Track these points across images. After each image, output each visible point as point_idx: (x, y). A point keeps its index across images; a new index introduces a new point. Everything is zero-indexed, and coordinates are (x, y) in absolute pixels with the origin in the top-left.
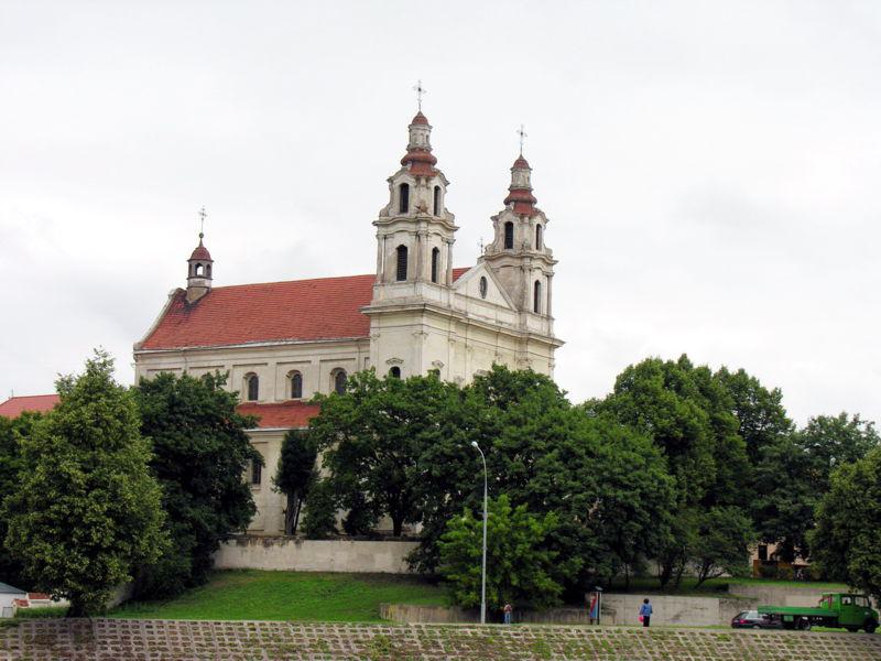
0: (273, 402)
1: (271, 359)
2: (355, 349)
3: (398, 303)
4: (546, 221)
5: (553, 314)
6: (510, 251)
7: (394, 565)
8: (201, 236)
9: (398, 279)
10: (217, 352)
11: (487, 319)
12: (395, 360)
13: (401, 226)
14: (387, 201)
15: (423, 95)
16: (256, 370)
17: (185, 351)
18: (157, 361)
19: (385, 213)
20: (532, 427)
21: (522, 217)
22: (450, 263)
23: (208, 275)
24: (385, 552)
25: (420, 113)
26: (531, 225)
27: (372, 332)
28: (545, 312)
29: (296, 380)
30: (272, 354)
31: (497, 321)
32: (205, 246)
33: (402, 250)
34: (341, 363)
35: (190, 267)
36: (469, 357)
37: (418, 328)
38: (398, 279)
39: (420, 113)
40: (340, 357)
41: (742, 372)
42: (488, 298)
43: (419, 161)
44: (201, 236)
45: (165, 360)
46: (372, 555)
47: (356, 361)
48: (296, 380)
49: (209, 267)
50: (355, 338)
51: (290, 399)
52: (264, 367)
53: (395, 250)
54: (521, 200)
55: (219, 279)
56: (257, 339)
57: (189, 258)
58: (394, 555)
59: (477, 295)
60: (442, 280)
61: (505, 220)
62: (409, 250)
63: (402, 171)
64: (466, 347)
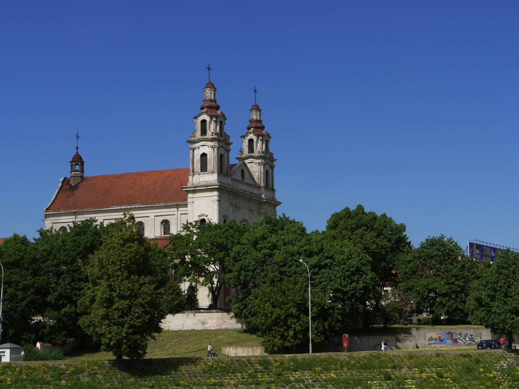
0: (154, 237)
1: (151, 213)
3: (202, 184)
4: (225, 119)
5: (275, 188)
6: (252, 154)
8: (77, 148)
9: (201, 172)
11: (245, 191)
12: (202, 215)
15: (210, 72)
17: (74, 212)
18: (58, 218)
20: (56, 294)
22: (228, 162)
27: (189, 200)
28: (271, 187)
29: (166, 224)
31: (250, 192)
34: (167, 217)
35: (72, 165)
36: (238, 212)
38: (201, 172)
40: (166, 214)
41: (384, 215)
42: (245, 181)
44: (77, 148)
47: (176, 215)
48: (166, 224)
49: (82, 165)
50: (175, 203)
51: (163, 235)
53: (200, 156)
56: (116, 205)
57: (71, 161)
59: (240, 178)
60: (225, 171)
62: (208, 156)
64: (236, 207)
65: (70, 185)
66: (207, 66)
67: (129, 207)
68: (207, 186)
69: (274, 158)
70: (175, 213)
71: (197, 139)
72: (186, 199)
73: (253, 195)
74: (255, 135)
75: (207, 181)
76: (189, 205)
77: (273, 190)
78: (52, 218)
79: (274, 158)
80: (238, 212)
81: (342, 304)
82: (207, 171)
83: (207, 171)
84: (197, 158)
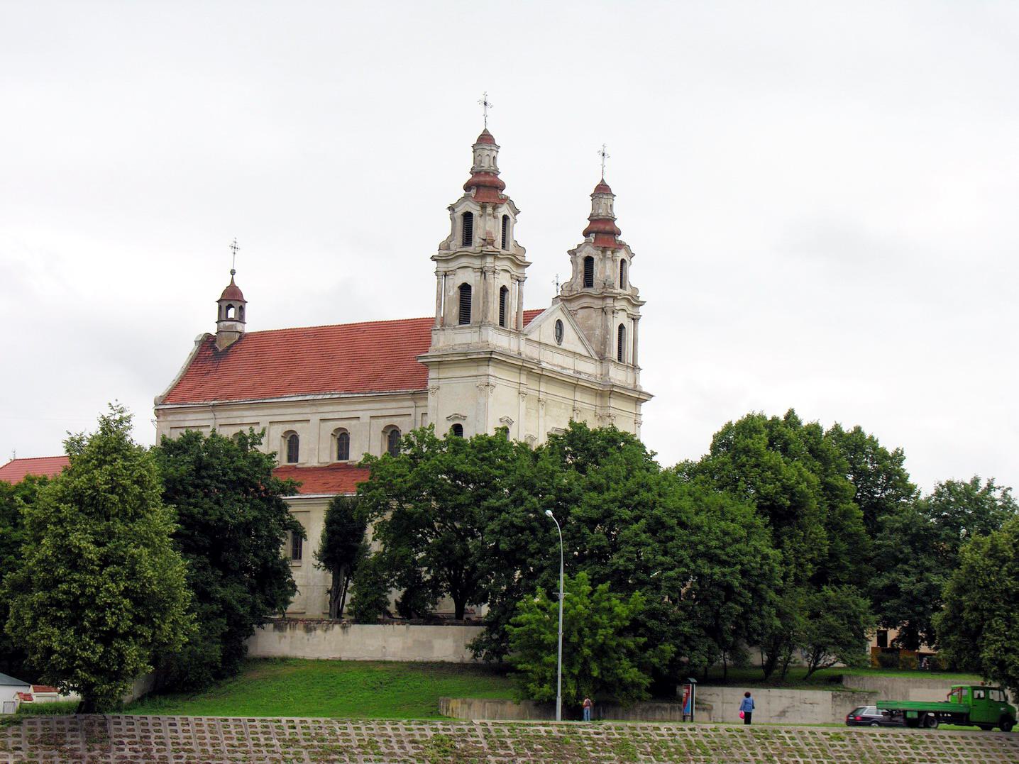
0: (316, 464)
2: (411, 403)
3: (459, 350)
5: (640, 364)
6: (589, 290)
7: (456, 652)
8: (233, 272)
9: (460, 323)
10: (251, 406)
11: (563, 368)
13: (464, 261)
14: (447, 231)
16: (296, 427)
17: (214, 405)
18: (181, 417)
19: (445, 246)
21: (604, 250)
22: (520, 304)
23: (241, 318)
24: (446, 638)
25: (485, 130)
26: (614, 261)
27: (431, 384)
29: (343, 439)
30: (314, 409)
31: (575, 371)
32: (237, 284)
33: (465, 289)
35: (220, 308)
36: (542, 412)
37: (484, 379)
38: (460, 323)
39: (485, 130)
40: (393, 412)
41: (858, 430)
42: (564, 345)
43: (485, 186)
44: (233, 272)
45: (191, 417)
46: (430, 642)
47: (413, 417)
48: (343, 439)
49: (242, 309)
50: (411, 391)
52: (305, 424)
53: (456, 289)
54: (602, 231)
55: (254, 323)
56: (297, 392)
57: (218, 298)
58: (455, 641)
61: (584, 254)
62: (473, 288)
63: (465, 198)
65: (215, 349)
66: (601, 149)
67: (320, 397)
68: (466, 354)
69: (640, 299)
70: (411, 411)
71: (452, 252)
72: (424, 383)
73: (583, 376)
74: (596, 248)
75: (468, 344)
76: (430, 396)
77: (635, 368)
78: (170, 418)
79: (640, 299)
80: (542, 412)
81: (975, 515)
82: (469, 322)
83: (469, 322)
84: (451, 294)
